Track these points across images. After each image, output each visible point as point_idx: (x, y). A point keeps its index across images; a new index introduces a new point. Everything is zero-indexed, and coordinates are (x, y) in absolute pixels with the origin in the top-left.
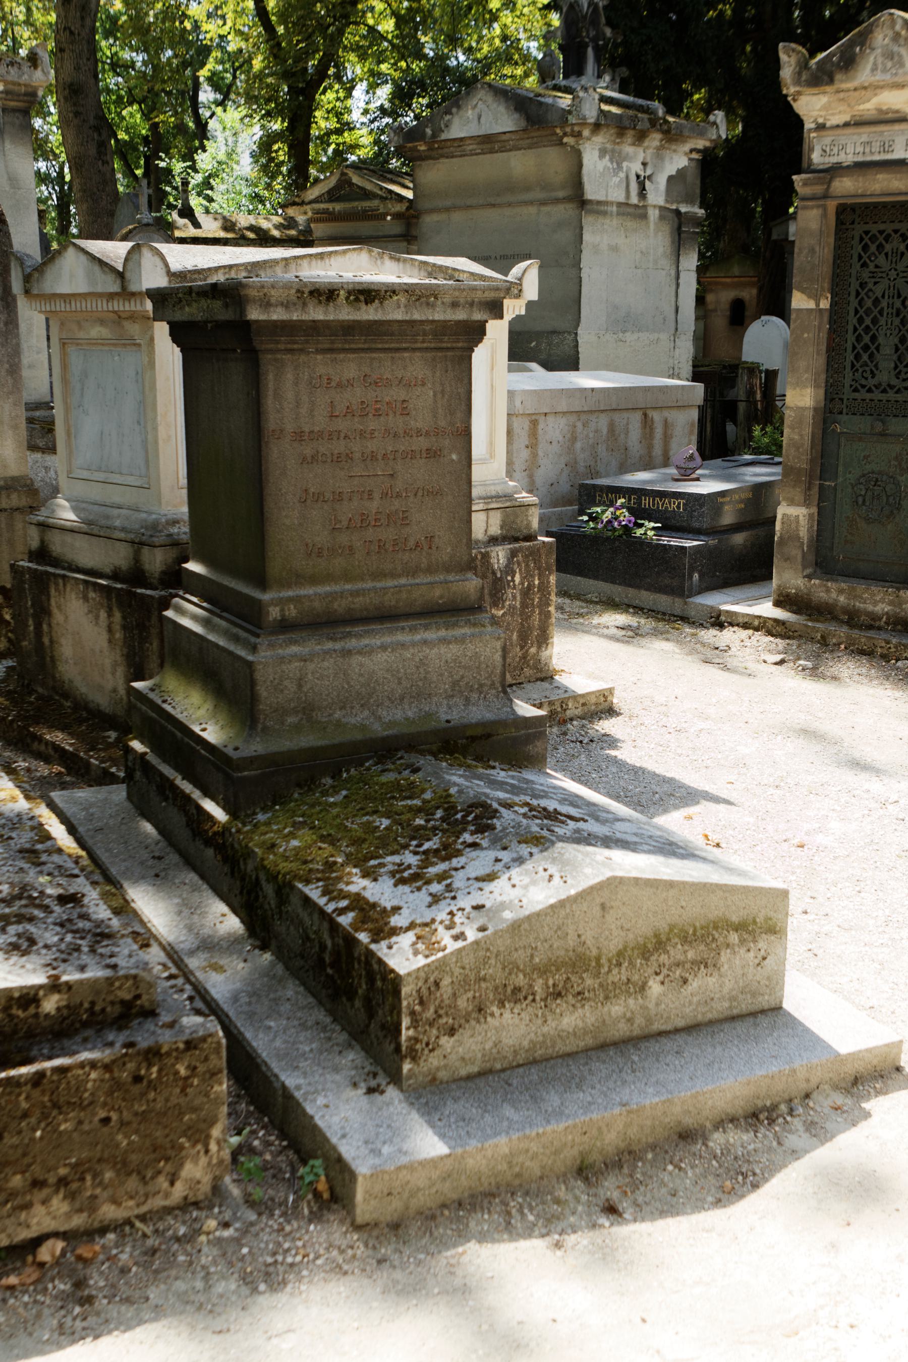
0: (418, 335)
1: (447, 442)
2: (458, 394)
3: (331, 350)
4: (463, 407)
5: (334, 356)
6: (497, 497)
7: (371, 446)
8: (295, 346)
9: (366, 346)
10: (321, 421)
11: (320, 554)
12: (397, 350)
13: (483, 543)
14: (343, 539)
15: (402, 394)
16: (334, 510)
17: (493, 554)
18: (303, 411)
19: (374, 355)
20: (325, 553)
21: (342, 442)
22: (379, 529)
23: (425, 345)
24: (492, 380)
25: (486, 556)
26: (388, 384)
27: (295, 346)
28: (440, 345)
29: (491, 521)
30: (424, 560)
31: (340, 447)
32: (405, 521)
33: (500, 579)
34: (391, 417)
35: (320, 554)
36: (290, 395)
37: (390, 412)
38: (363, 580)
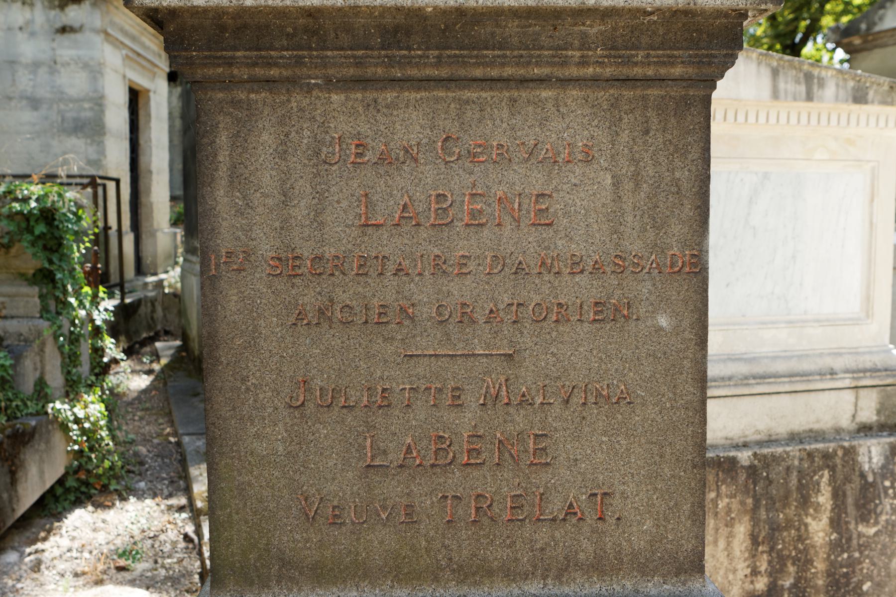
0: (567, 46)
1: (645, 288)
2: (676, 182)
3: (362, 83)
4: (688, 210)
5: (370, 95)
6: (874, 370)
7: (459, 290)
8: (274, 72)
9: (444, 72)
10: (340, 236)
11: (336, 521)
12: (523, 82)
13: (849, 432)
14: (392, 489)
15: (537, 181)
16: (371, 427)
17: (862, 450)
18: (300, 211)
19: (467, 94)
20: (350, 516)
21: (391, 282)
22: (476, 473)
23: (590, 71)
24: (871, 214)
25: (850, 453)
26: (504, 158)
27: (274, 72)
28: (626, 71)
29: (861, 404)
30: (585, 544)
31: (386, 292)
32: (542, 460)
33: (873, 485)
34: (507, 231)
35: (336, 521)
36: (268, 179)
37: (507, 219)
38: (436, 579)
